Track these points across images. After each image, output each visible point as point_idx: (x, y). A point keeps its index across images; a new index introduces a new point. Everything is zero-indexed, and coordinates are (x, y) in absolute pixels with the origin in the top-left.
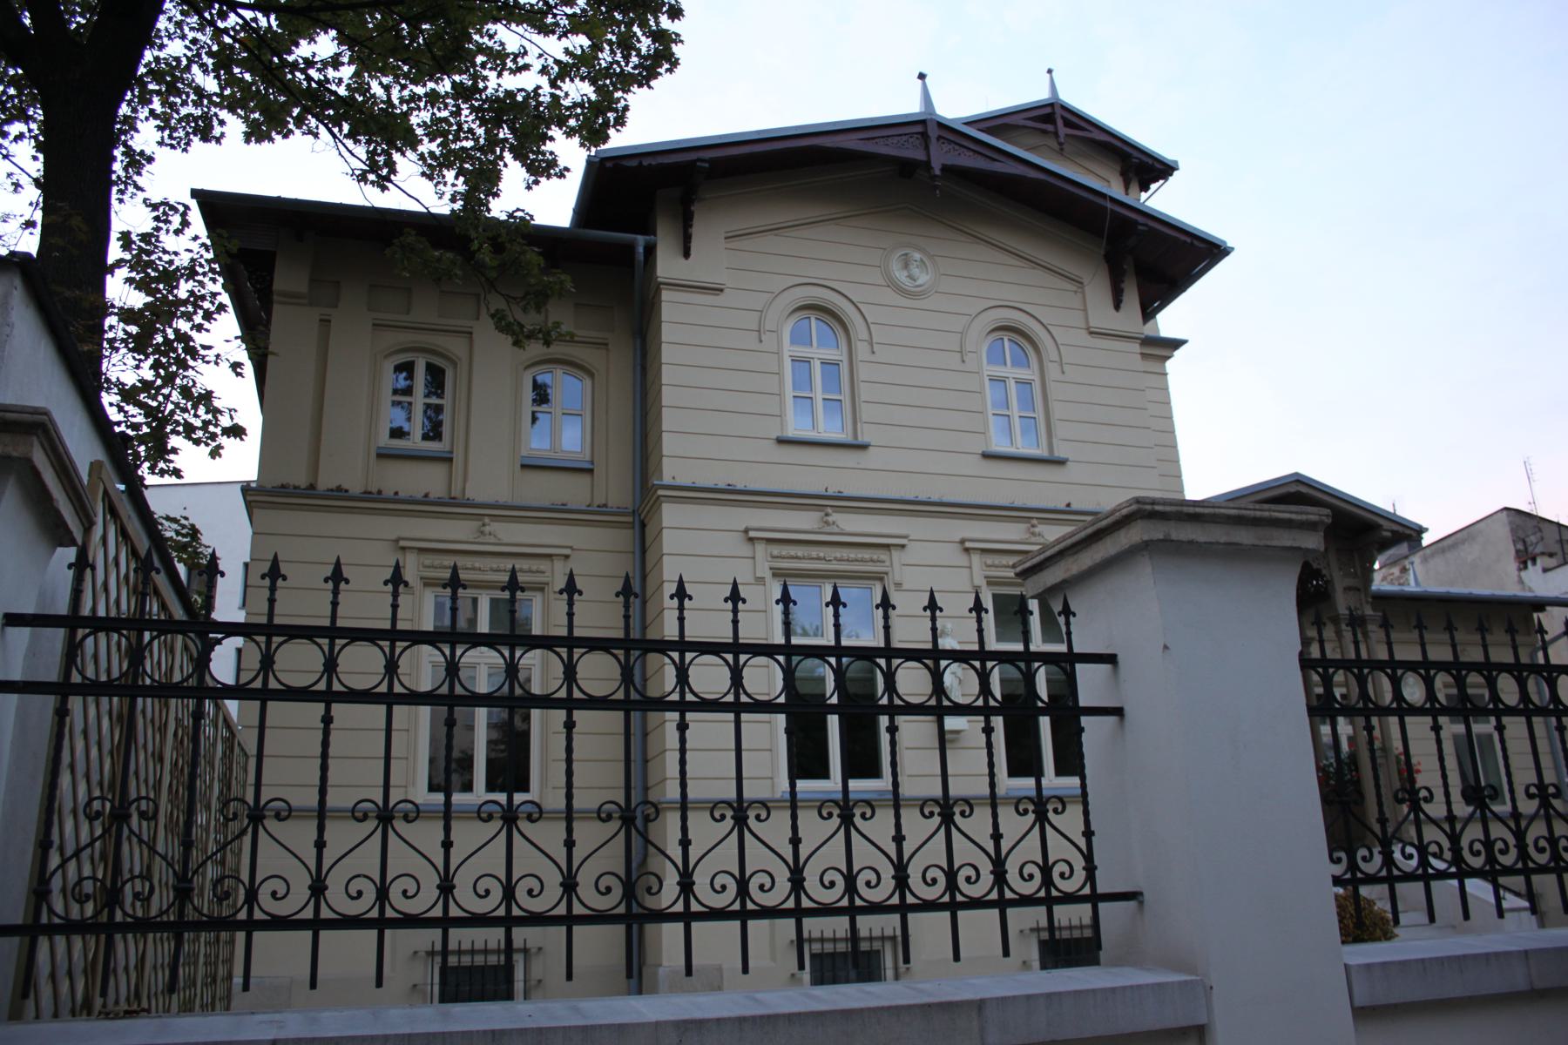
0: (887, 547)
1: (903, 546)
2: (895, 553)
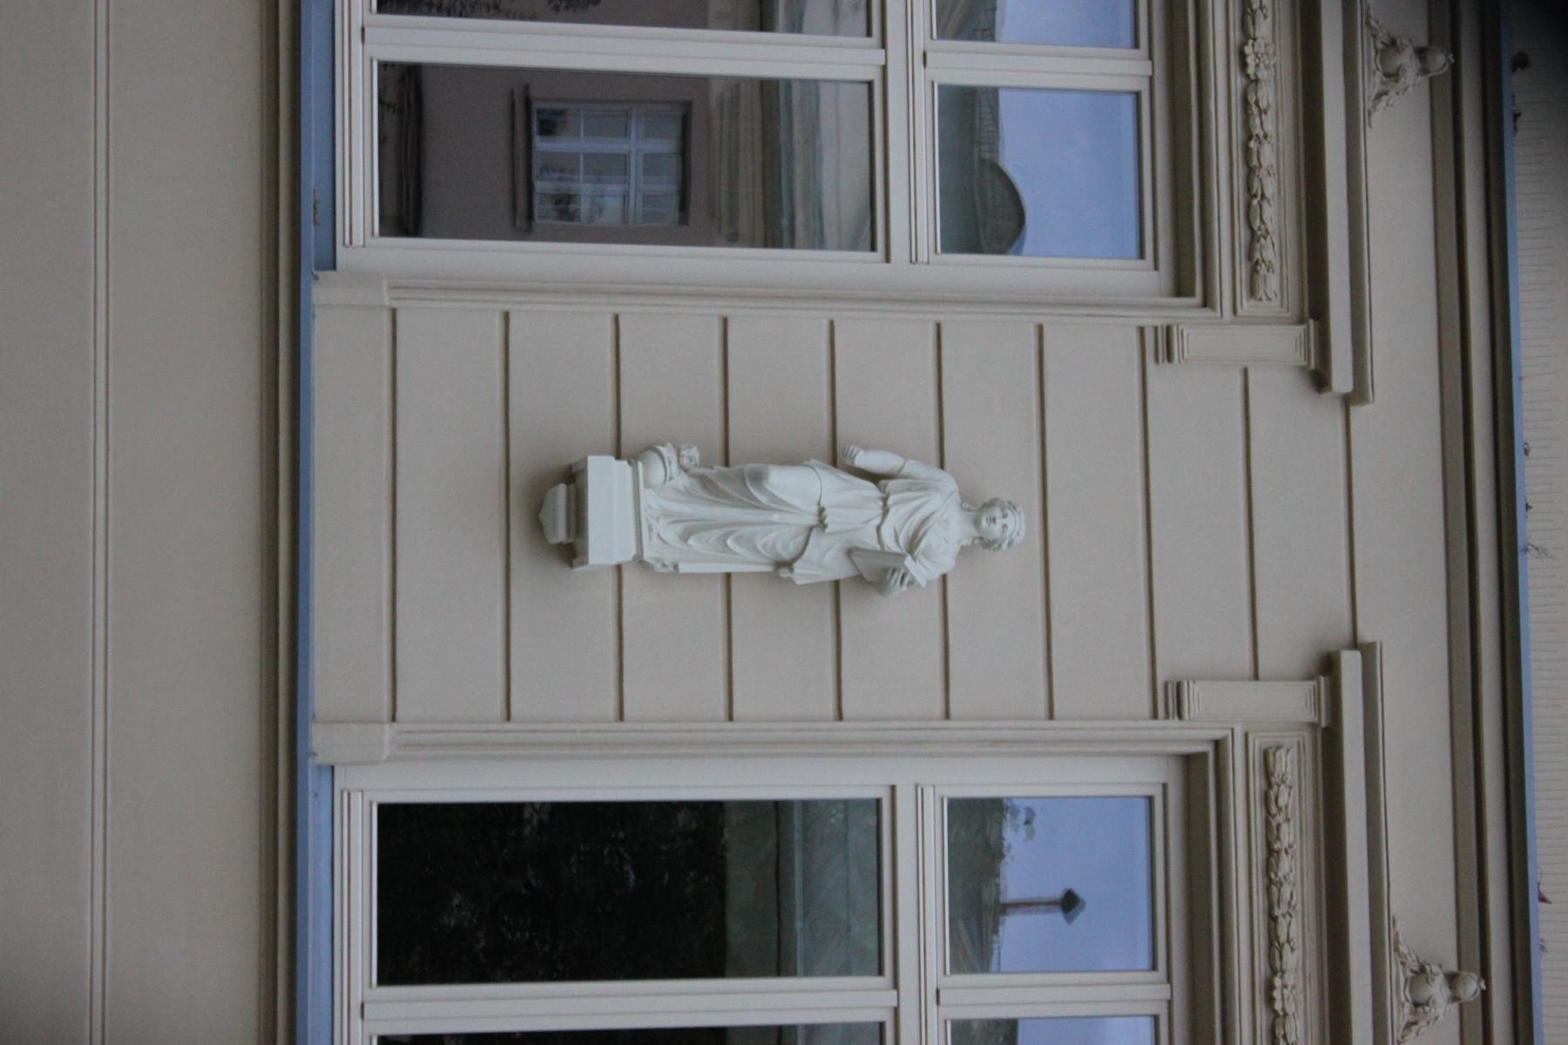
0: (1315, 308)
1: (1320, 379)
2: (1283, 343)
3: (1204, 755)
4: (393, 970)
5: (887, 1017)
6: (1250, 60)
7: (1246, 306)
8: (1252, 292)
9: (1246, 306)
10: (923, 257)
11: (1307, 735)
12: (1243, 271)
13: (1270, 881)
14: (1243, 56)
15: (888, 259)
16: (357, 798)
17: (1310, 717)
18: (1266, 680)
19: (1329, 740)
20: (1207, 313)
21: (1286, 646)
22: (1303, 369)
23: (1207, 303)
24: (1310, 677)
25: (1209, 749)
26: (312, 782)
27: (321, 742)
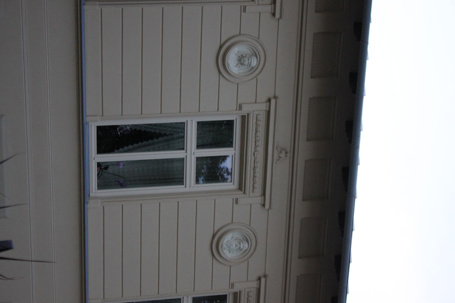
1: (274, 14)
2: (259, 200)
3: (245, 116)
4: (100, 151)
5: (185, 157)
6: (255, 155)
7: (250, 195)
8: (253, 191)
9: (251, 194)
10: (192, 186)
11: (265, 112)
12: (251, 188)
13: (254, 167)
14: (254, 154)
15: (186, 187)
16: (93, 126)
17: (256, 286)
18: (258, 103)
19: (259, 290)
20: (244, 195)
21: (263, 98)
22: (261, 204)
23: (244, 193)
24: (266, 102)
25: (247, 115)
26: (86, 126)
27: (87, 119)
